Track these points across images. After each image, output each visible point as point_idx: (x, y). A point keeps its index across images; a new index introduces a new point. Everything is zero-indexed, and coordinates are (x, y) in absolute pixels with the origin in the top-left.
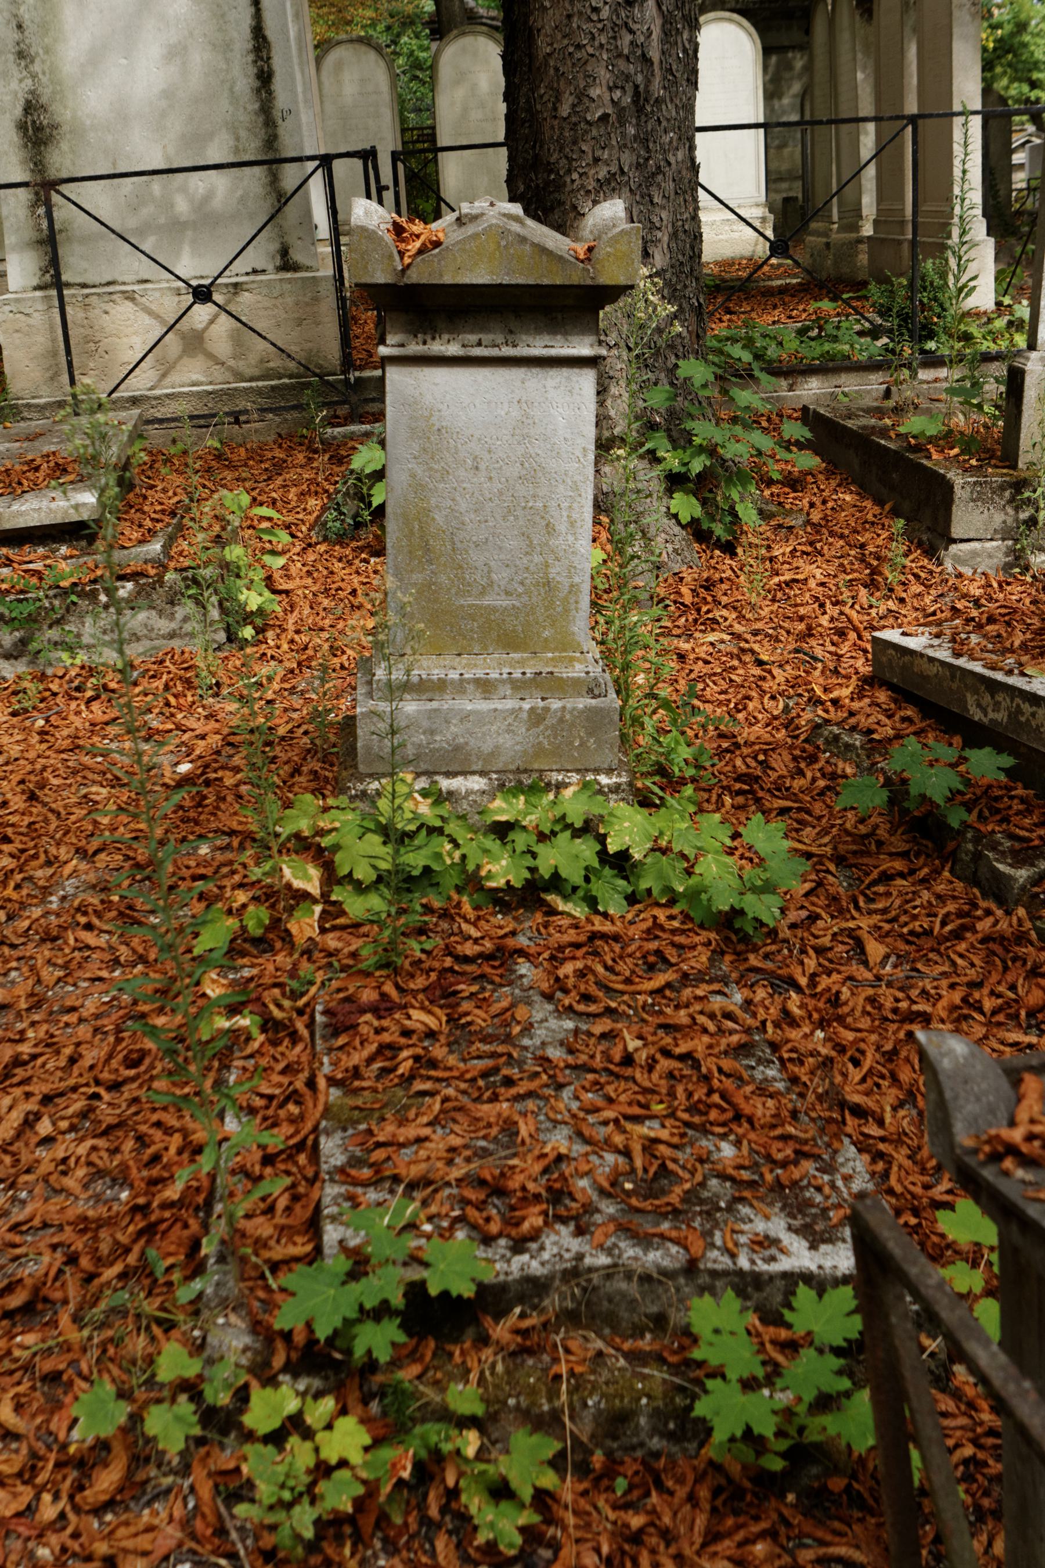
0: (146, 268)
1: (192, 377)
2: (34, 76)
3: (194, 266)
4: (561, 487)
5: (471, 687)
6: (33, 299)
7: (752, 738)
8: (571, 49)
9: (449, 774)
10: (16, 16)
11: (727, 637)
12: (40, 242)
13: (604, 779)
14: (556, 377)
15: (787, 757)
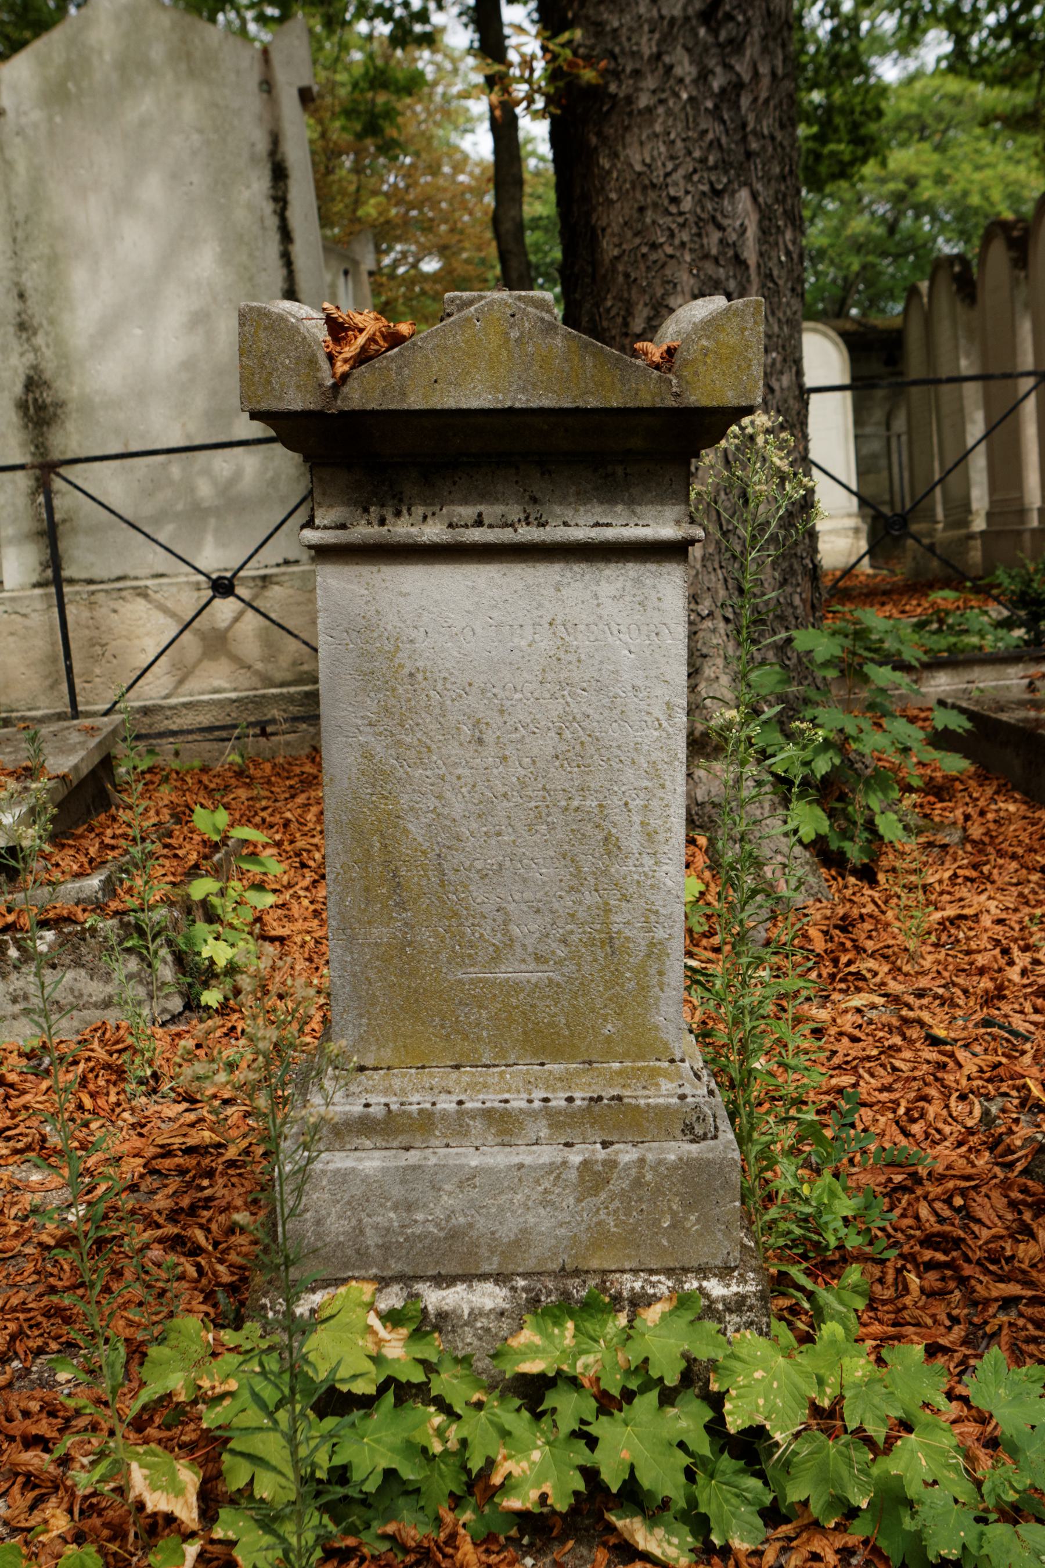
0: (160, 560)
1: (217, 683)
2: (36, 350)
3: (215, 558)
4: (629, 773)
5: (477, 1125)
6: (31, 597)
7: (940, 1168)
8: (645, 250)
9: (443, 1281)
10: (17, 284)
11: (880, 1001)
12: (40, 534)
13: (716, 1288)
14: (613, 581)
15: (1000, 1202)
